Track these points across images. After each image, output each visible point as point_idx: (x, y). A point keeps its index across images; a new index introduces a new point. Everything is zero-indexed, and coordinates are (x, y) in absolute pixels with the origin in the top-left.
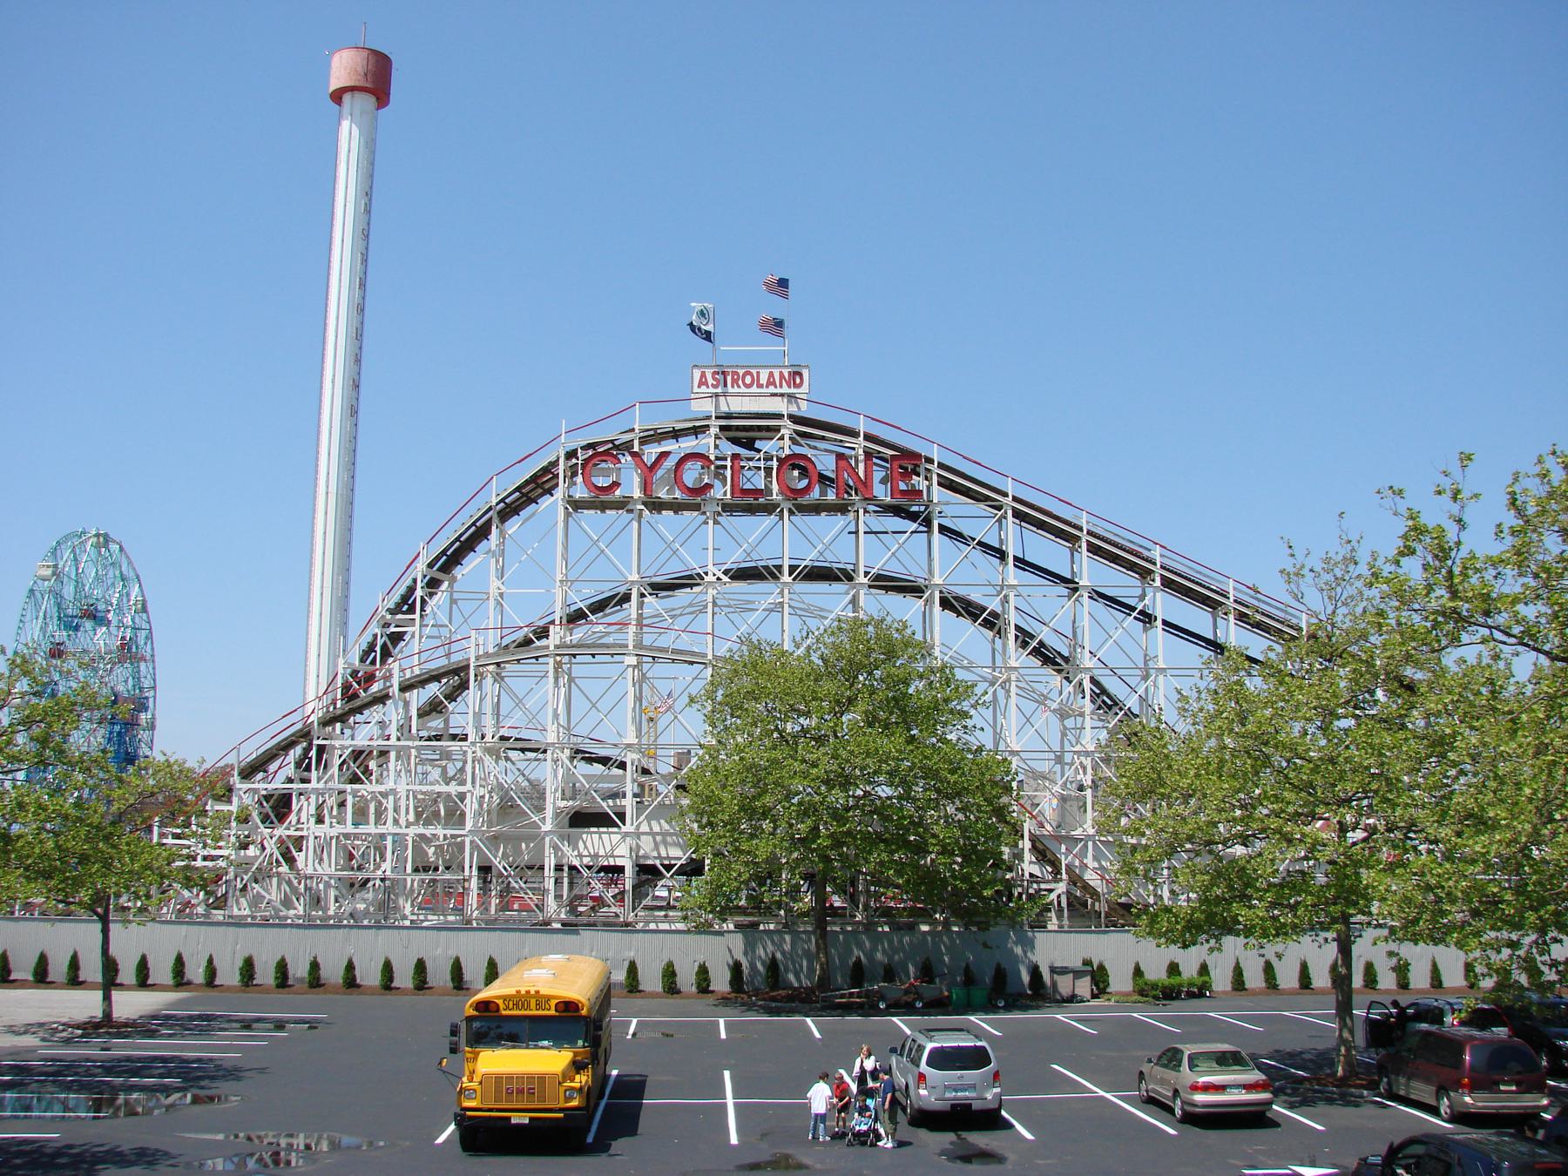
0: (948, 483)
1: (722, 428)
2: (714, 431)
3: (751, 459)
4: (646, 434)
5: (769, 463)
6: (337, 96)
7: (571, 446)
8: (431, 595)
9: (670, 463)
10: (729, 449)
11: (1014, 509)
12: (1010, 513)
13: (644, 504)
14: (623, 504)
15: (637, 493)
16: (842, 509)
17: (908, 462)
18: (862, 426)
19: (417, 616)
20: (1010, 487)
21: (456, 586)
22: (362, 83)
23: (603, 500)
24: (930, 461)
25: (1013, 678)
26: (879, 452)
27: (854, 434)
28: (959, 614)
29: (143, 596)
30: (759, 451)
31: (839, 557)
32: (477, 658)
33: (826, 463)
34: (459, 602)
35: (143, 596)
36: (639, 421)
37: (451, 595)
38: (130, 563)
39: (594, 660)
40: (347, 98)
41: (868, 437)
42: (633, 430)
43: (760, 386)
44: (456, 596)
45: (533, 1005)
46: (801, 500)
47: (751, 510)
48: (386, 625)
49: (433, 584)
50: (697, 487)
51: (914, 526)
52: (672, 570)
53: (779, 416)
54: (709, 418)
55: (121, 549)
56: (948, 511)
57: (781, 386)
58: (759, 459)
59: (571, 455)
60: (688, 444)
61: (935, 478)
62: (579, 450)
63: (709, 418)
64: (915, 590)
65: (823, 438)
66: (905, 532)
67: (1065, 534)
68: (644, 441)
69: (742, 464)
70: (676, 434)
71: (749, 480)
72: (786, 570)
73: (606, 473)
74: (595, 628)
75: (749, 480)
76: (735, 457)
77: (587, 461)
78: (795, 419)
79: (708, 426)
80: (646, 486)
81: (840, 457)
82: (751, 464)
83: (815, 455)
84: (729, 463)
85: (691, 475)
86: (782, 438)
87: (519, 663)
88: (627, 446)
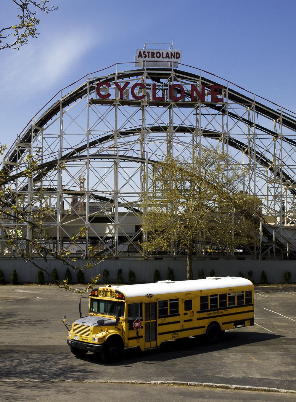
1: (149, 74)
3: (160, 86)
9: (130, 86)
17: (217, 89)
23: (104, 101)
24: (226, 88)
33: (187, 88)
37: (43, 136)
39: (102, 161)
42: (115, 74)
43: (163, 58)
45: (243, 294)
46: (178, 102)
47: (158, 105)
48: (19, 147)
49: (36, 131)
50: (106, 95)
57: (171, 58)
59: (91, 82)
67: (272, 115)
79: (143, 73)
87: (74, 162)
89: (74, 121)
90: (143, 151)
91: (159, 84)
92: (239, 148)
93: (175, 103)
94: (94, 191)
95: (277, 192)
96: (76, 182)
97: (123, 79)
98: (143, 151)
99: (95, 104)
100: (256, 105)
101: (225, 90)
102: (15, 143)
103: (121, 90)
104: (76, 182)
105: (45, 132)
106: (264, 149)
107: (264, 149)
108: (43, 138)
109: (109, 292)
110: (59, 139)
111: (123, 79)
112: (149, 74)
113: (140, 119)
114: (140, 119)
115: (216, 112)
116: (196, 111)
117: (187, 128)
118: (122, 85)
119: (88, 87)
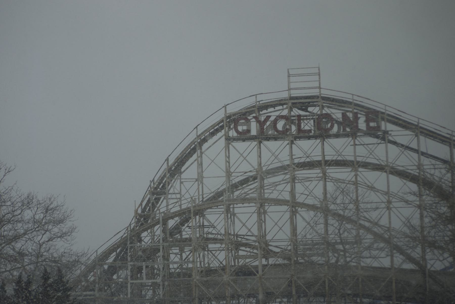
34: (184, 183)
37: (180, 180)
44: (182, 180)
89: (245, 161)
90: (292, 193)
91: (307, 113)
94: (242, 237)
95: (369, 157)
96: (307, 189)
97: (267, 110)
98: (292, 193)
101: (382, 115)
102: (148, 191)
104: (307, 189)
105: (183, 176)
108: (181, 183)
110: (197, 182)
111: (267, 110)
115: (375, 140)
116: (354, 142)
118: (262, 119)
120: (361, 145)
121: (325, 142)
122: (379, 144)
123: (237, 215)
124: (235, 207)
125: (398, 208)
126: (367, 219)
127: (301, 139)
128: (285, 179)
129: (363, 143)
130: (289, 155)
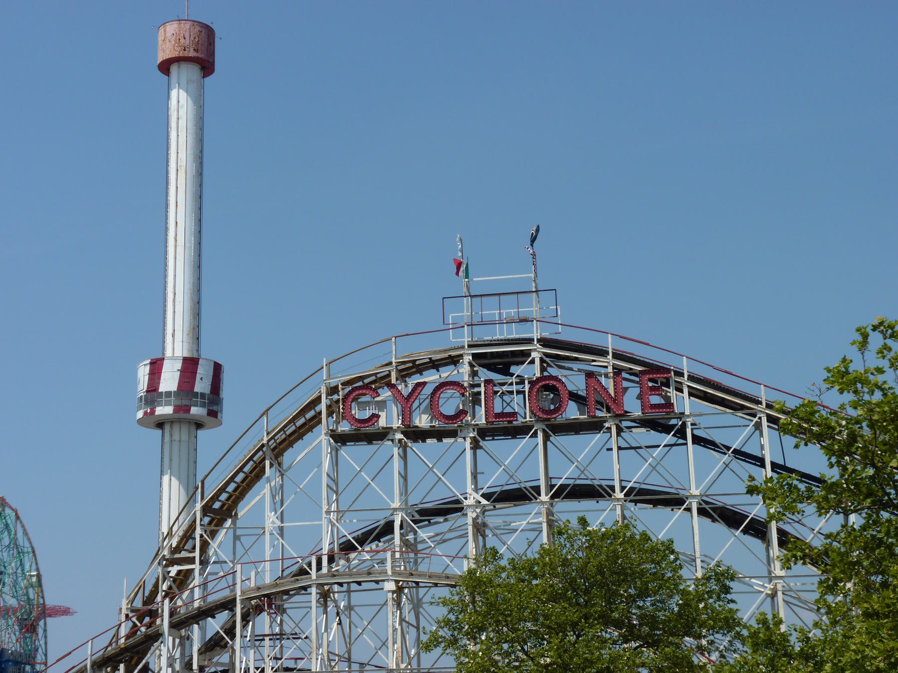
0: (702, 395)
1: (474, 356)
2: (468, 358)
4: (403, 367)
5: (476, 390)
6: (165, 67)
7: (333, 382)
8: (213, 534)
10: (484, 374)
11: (768, 416)
12: (764, 420)
13: (402, 433)
14: (383, 435)
15: (397, 423)
16: (595, 426)
18: (610, 343)
19: (197, 554)
20: (763, 393)
21: (239, 524)
22: (192, 54)
24: (680, 374)
25: (779, 587)
26: (631, 369)
27: (603, 353)
28: (714, 520)
29: (38, 570)
30: (512, 375)
31: (596, 475)
32: (243, 593)
33: (575, 382)
34: (242, 538)
35: (38, 570)
36: (396, 353)
37: (235, 532)
38: (26, 533)
40: (174, 69)
41: (616, 356)
42: (390, 364)
44: (239, 532)
51: (669, 438)
52: (434, 499)
53: (529, 341)
54: (463, 347)
55: (18, 517)
56: (703, 422)
58: (511, 384)
59: (333, 390)
60: (446, 373)
61: (686, 390)
62: (340, 386)
63: (463, 347)
64: (675, 501)
65: (576, 359)
66: (658, 446)
68: (404, 374)
69: (496, 389)
70: (435, 365)
71: (508, 404)
72: (617, 489)
73: (363, 406)
74: (363, 556)
75: (508, 404)
76: (488, 382)
77: (346, 397)
78: (545, 342)
80: (406, 415)
81: (590, 375)
82: (505, 388)
83: (565, 376)
84: (482, 389)
85: (450, 403)
86: (532, 362)
88: (384, 381)
92: (548, 360)
93: (547, 426)
99: (353, 443)
100: (767, 413)
103: (406, 403)
106: (660, 461)
107: (660, 461)
109: (687, 412)
112: (474, 356)
113: (483, 473)
114: (483, 473)
117: (592, 486)
118: (406, 392)
119: (323, 407)
120: (631, 448)
121: (549, 443)
122: (672, 445)
123: (356, 608)
124: (352, 589)
125: (381, 608)
126: (402, 644)
127: (496, 438)
128: (456, 528)
129: (634, 445)
130: (598, 502)
